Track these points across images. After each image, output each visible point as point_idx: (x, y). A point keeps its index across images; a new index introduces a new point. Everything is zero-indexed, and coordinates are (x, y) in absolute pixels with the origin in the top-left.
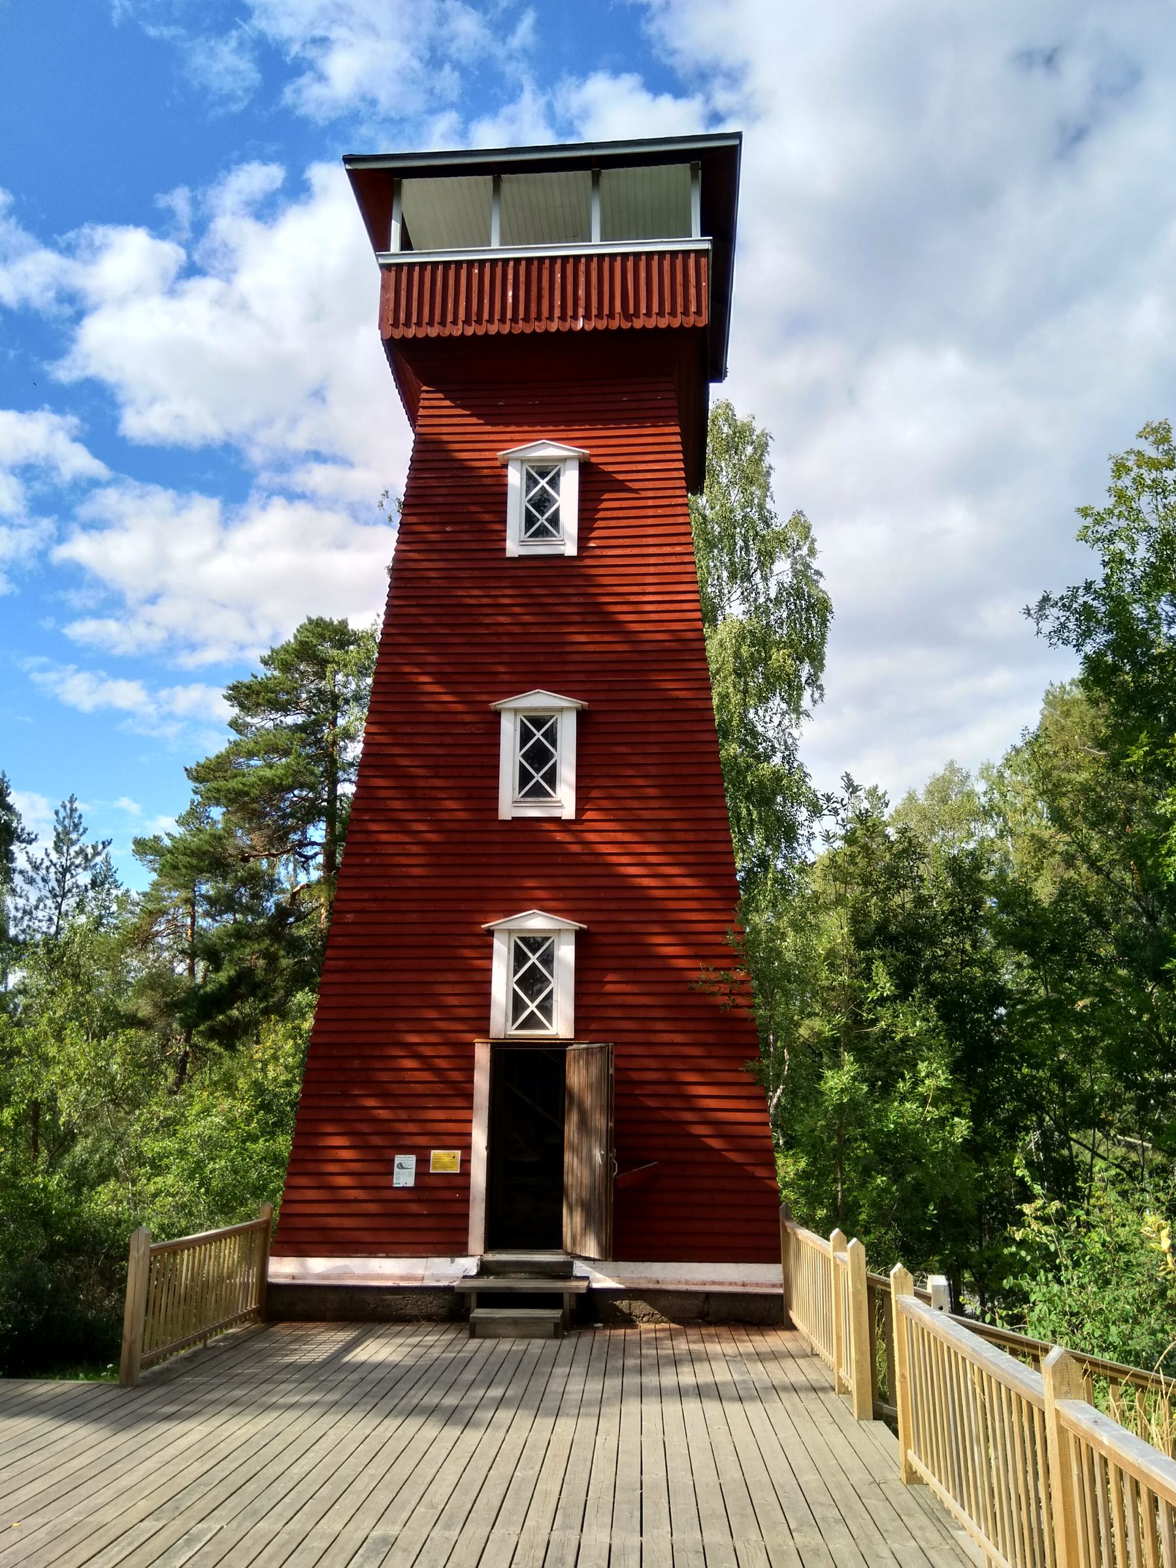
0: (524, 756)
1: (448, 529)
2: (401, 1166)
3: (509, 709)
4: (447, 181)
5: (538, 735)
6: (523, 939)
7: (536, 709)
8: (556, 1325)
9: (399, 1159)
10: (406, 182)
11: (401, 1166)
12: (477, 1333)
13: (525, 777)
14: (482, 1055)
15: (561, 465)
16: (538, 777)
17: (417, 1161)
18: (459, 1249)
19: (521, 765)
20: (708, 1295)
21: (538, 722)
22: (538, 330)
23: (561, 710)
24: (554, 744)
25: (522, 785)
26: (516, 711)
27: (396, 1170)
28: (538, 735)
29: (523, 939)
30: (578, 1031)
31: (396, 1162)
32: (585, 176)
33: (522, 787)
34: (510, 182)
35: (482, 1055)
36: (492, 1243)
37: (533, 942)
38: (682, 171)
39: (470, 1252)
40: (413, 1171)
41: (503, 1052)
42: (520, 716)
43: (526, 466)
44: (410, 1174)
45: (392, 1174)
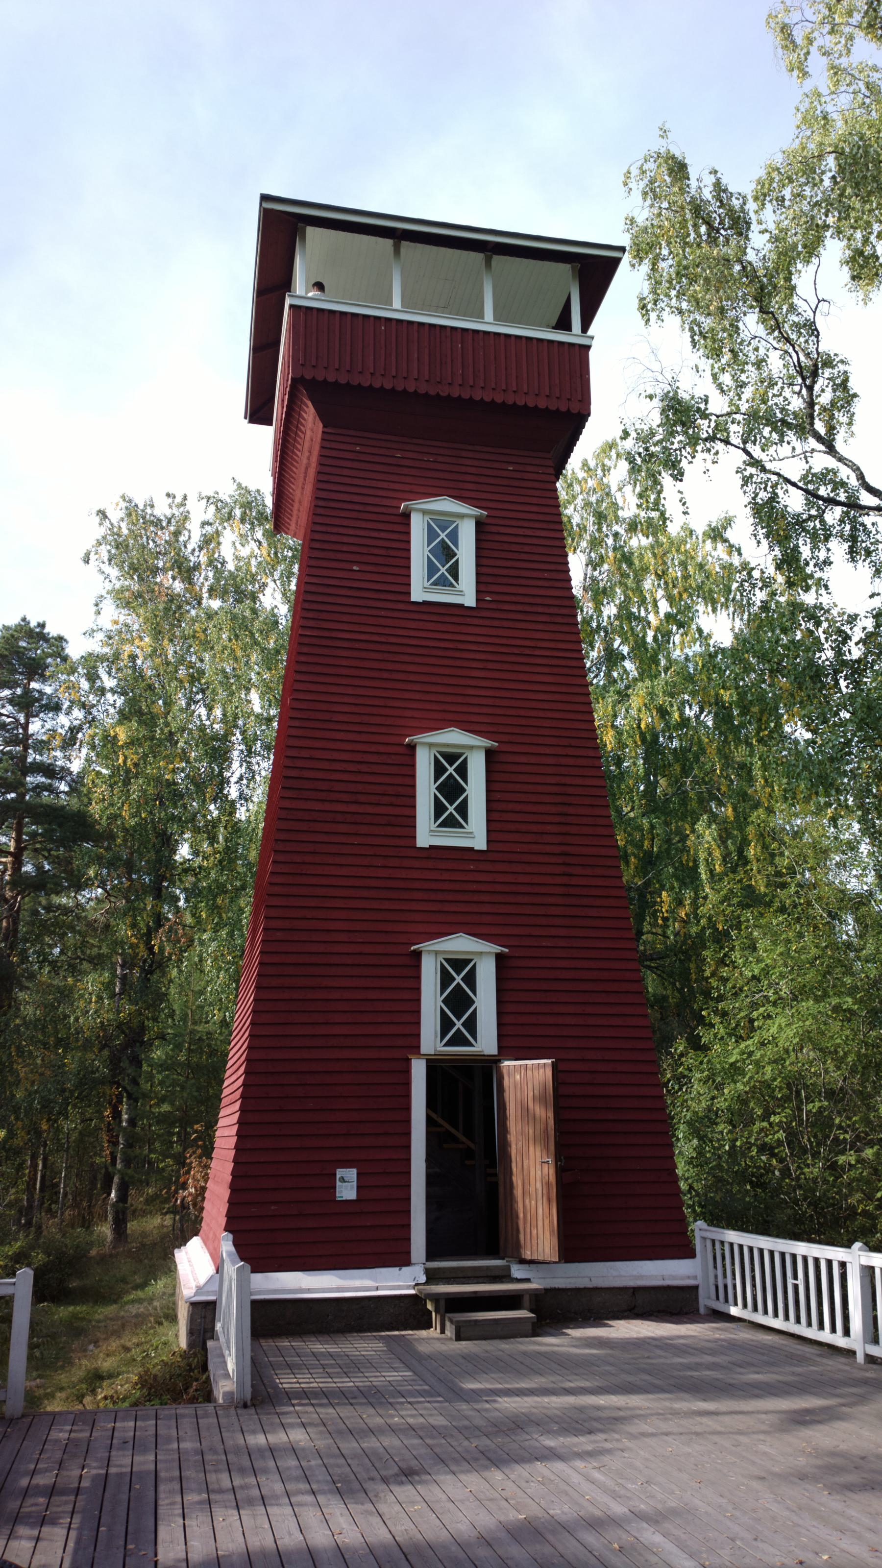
0: (465, 790)
1: (355, 568)
2: (343, 1180)
3: (429, 952)
4: (434, 249)
5: (451, 770)
6: (448, 960)
7: (448, 745)
8: (533, 1323)
9: (340, 1173)
10: (310, 231)
11: (343, 1180)
12: (462, 1335)
13: (439, 809)
14: (418, 1071)
15: (458, 521)
16: (451, 809)
17: (358, 1174)
18: (402, 1260)
19: (436, 796)
20: (636, 1290)
21: (451, 758)
22: (442, 394)
23: (471, 748)
24: (465, 778)
25: (437, 816)
26: (431, 745)
27: (338, 1183)
28: (451, 770)
29: (448, 960)
30: (500, 1048)
31: (338, 1176)
32: (478, 257)
33: (437, 817)
34: (498, 261)
35: (418, 1071)
36: (432, 1254)
37: (459, 964)
38: (564, 269)
39: (413, 1261)
40: (355, 1184)
41: (434, 1067)
42: (434, 751)
43: (427, 518)
44: (352, 1187)
45: (335, 1188)
